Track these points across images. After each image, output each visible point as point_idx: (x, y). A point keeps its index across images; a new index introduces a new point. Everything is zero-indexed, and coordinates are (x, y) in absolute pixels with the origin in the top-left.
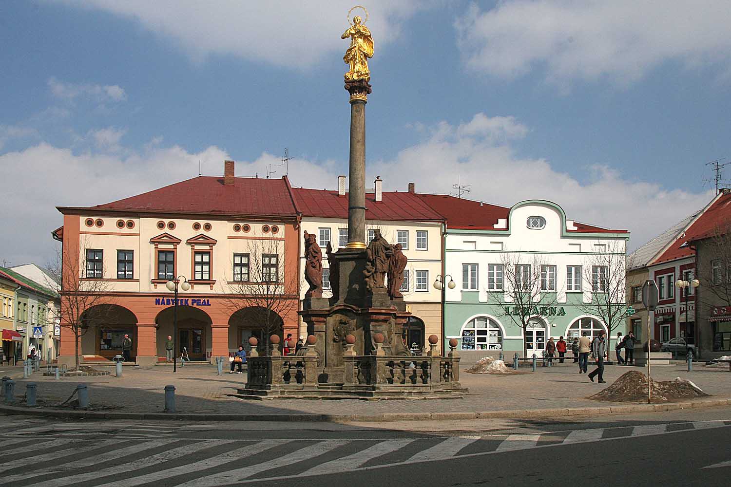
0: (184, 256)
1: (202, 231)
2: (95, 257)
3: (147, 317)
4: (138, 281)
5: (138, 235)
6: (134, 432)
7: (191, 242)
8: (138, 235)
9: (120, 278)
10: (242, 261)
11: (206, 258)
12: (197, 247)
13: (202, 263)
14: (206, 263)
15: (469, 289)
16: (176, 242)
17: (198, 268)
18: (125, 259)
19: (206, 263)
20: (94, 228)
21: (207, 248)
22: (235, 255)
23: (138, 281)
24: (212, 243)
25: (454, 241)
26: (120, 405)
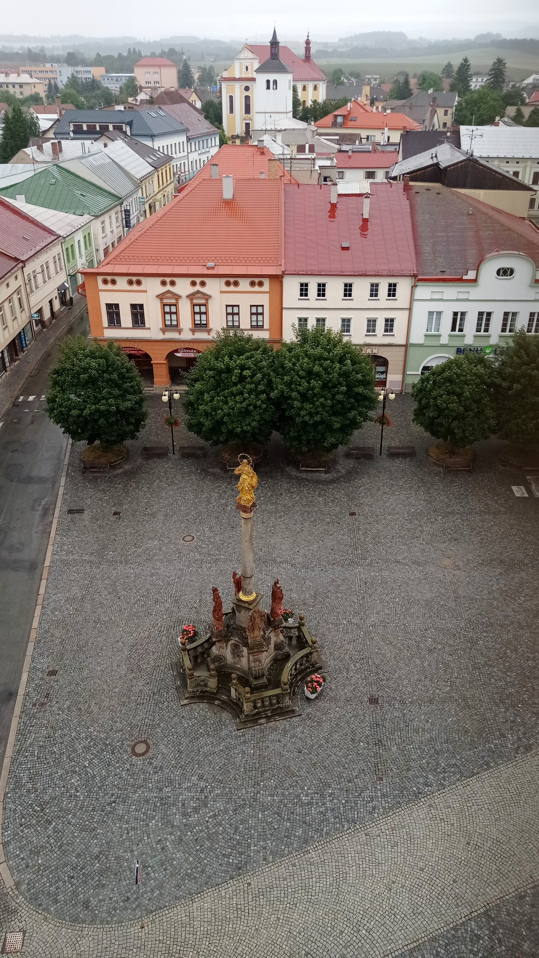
0: (185, 310)
1: (198, 288)
2: (113, 310)
3: (159, 359)
4: (149, 329)
5: (146, 291)
6: (68, 255)
7: (191, 297)
8: (146, 291)
9: (134, 327)
10: (232, 311)
11: (173, 309)
12: (166, 301)
13: (171, 313)
14: (174, 313)
15: (433, 333)
16: (177, 297)
17: (168, 317)
18: (138, 313)
19: (174, 313)
20: (110, 286)
21: (173, 301)
22: (227, 306)
23: (149, 329)
24: (207, 297)
25: (424, 291)
26: (209, 598)
